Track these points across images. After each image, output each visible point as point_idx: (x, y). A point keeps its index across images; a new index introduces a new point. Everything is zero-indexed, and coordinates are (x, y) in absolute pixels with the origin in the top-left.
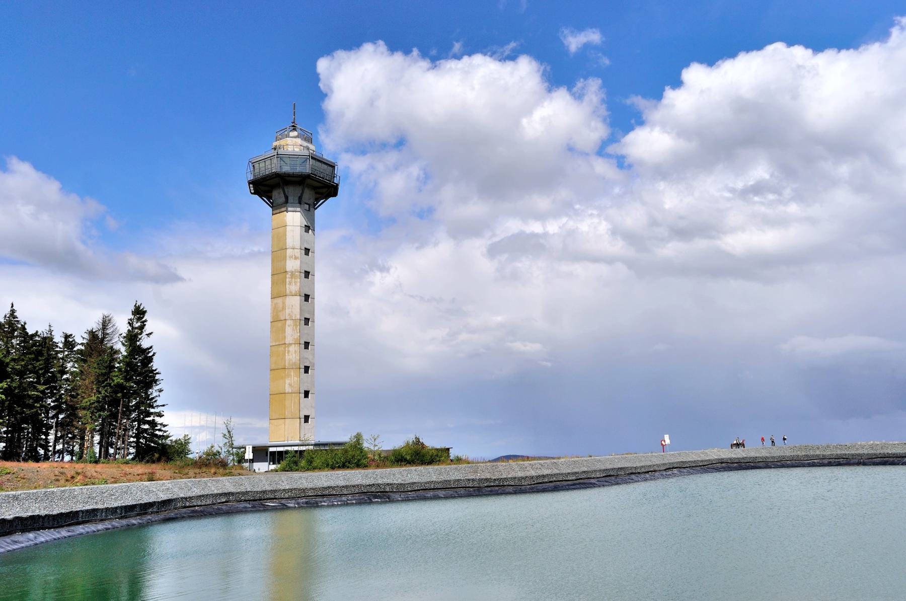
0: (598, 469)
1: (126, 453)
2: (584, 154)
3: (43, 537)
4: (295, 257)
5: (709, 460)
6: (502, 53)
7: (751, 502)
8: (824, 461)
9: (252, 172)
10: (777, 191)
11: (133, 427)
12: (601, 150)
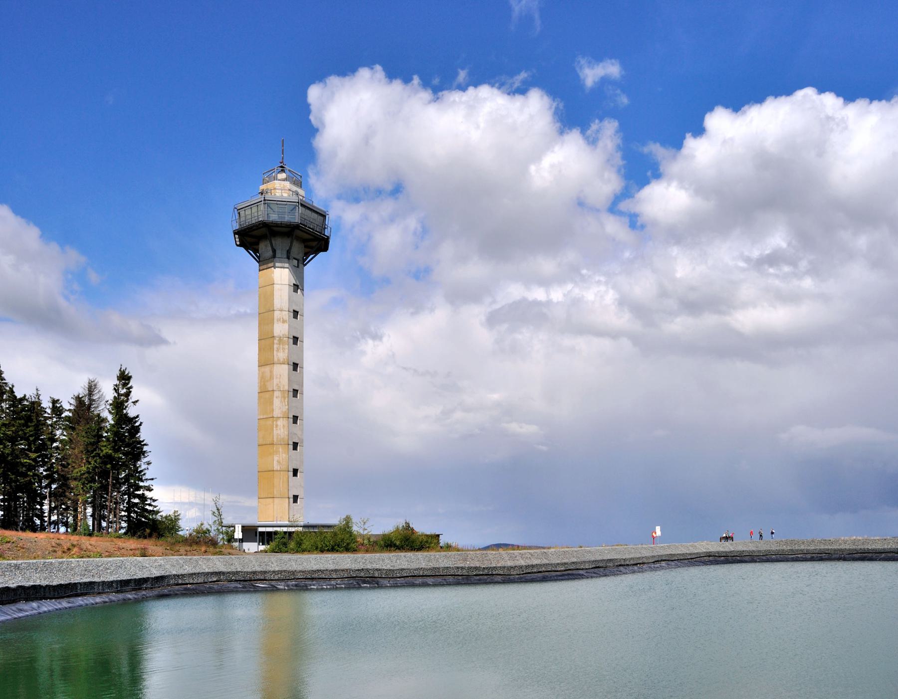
0: (588, 560)
1: (118, 527)
2: (595, 210)
3: (46, 607)
4: (283, 321)
5: (698, 553)
6: (511, 85)
7: (733, 596)
8: (807, 555)
9: (238, 221)
10: (793, 263)
11: (124, 501)
12: (613, 208)
